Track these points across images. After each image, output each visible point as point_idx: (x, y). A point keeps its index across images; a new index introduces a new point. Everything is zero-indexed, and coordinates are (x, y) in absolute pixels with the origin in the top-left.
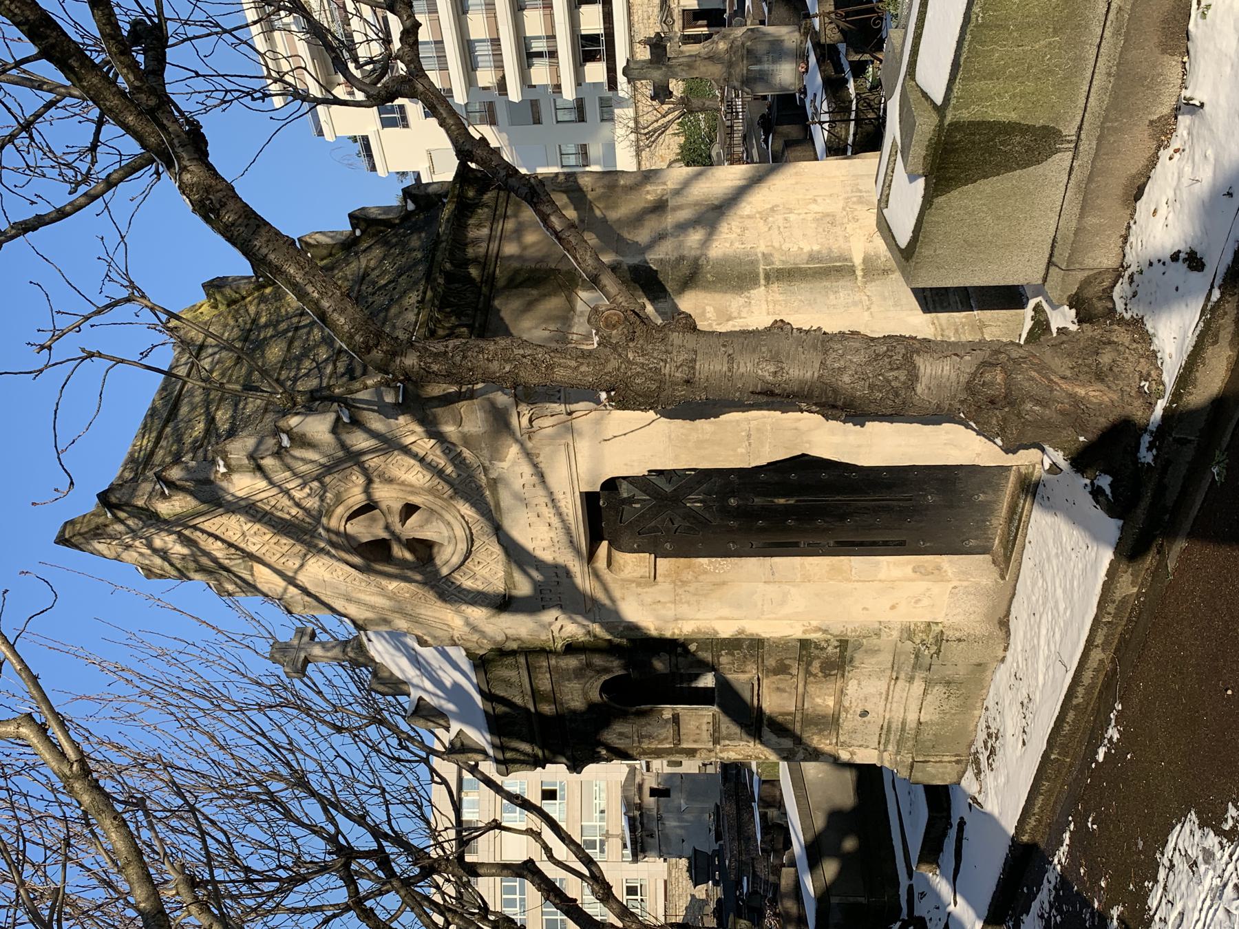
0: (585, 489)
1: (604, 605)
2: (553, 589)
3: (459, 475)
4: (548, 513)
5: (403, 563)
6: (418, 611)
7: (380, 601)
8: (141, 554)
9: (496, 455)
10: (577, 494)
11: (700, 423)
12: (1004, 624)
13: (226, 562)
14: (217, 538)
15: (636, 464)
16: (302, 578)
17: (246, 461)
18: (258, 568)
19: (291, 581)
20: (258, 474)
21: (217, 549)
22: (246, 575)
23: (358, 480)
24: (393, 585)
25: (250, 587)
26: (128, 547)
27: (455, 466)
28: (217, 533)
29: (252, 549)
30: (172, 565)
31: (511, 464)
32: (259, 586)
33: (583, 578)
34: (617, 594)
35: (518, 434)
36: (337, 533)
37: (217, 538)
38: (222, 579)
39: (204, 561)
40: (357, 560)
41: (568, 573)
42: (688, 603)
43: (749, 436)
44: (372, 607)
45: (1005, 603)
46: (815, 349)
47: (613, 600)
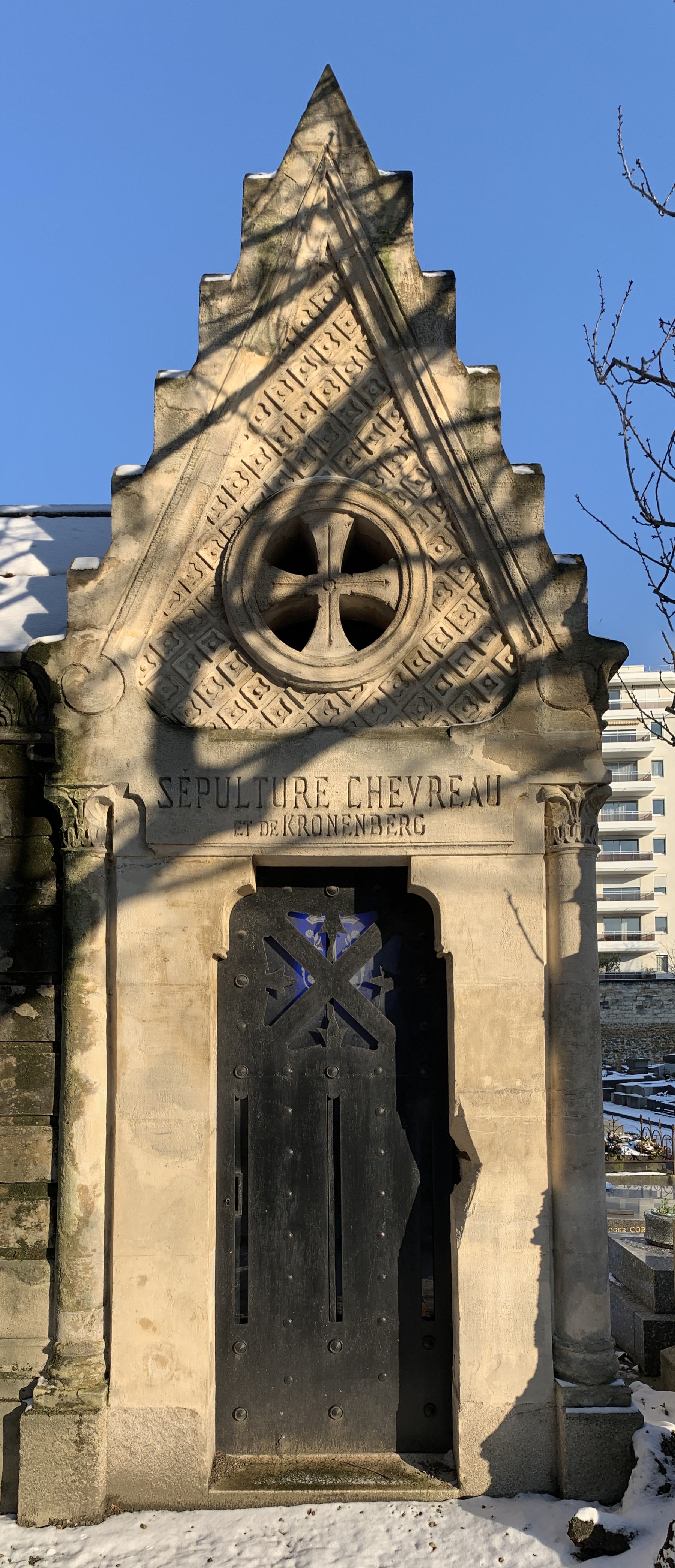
0: (416, 864)
1: (158, 873)
2: (195, 797)
3: (443, 692)
4: (382, 807)
5: (265, 582)
6: (154, 583)
7: (179, 529)
8: (303, 190)
9: (498, 745)
10: (411, 852)
11: (537, 1029)
12: (114, 1507)
13: (274, 317)
14: (317, 322)
15: (464, 937)
16: (231, 424)
17: (491, 404)
18: (255, 364)
19: (231, 404)
20: (465, 414)
21: (296, 313)
22: (252, 336)
23: (439, 551)
24: (211, 555)
25: (225, 335)
26: (321, 174)
27: (461, 689)
28: (328, 325)
29: (295, 364)
30: (278, 230)
31: (476, 761)
32: (226, 351)
33: (233, 846)
34: (185, 896)
35: (536, 780)
36: (339, 498)
37: (317, 322)
38: (241, 299)
39: (281, 285)
40: (280, 510)
41: (243, 824)
42: (163, 1004)
43: (514, 1090)
44: (169, 512)
45: (157, 1499)
46: (60, 1356)
47: (171, 887)
